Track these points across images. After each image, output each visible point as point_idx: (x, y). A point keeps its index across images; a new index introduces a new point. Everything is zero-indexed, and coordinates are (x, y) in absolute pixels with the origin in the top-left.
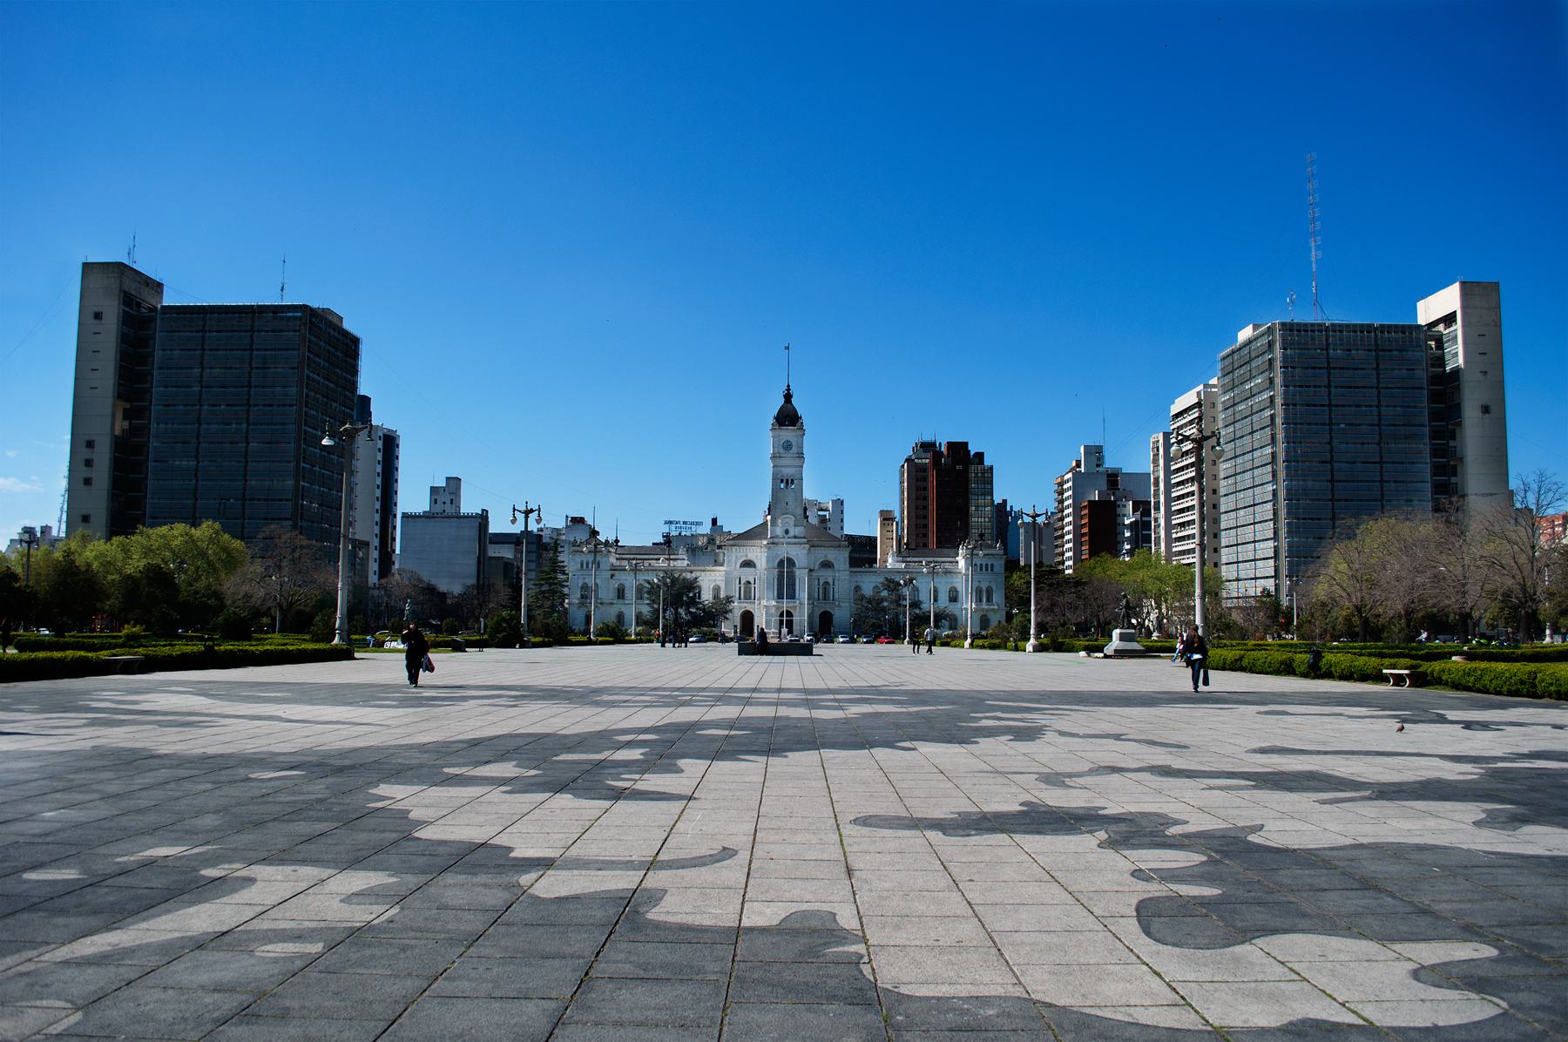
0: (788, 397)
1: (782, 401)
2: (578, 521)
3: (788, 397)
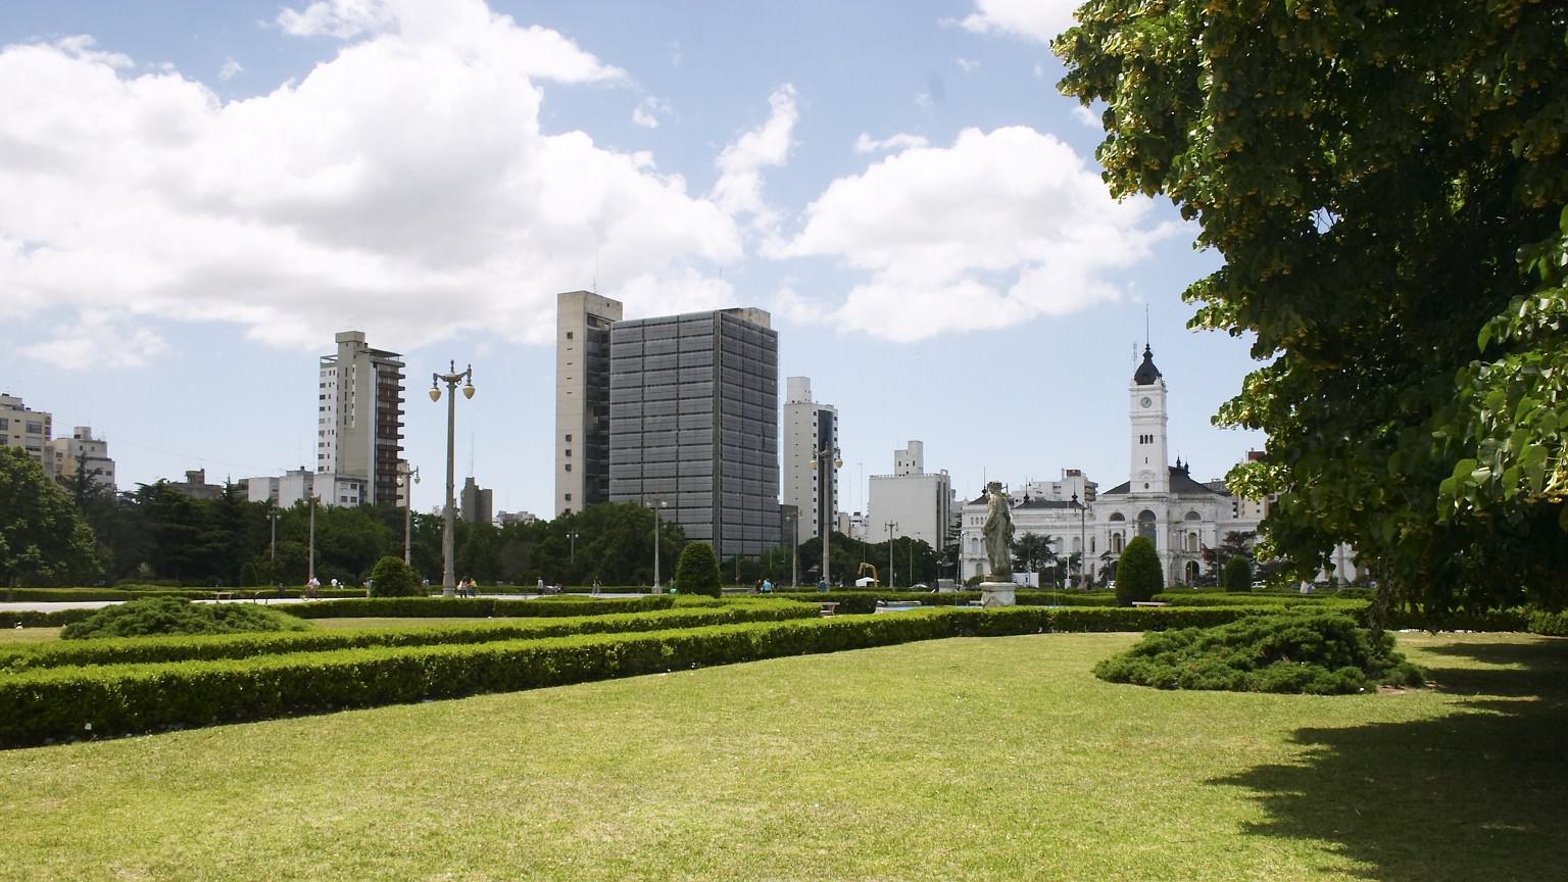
0: (1148, 355)
1: (1141, 360)
2: (1074, 473)
3: (1148, 355)
